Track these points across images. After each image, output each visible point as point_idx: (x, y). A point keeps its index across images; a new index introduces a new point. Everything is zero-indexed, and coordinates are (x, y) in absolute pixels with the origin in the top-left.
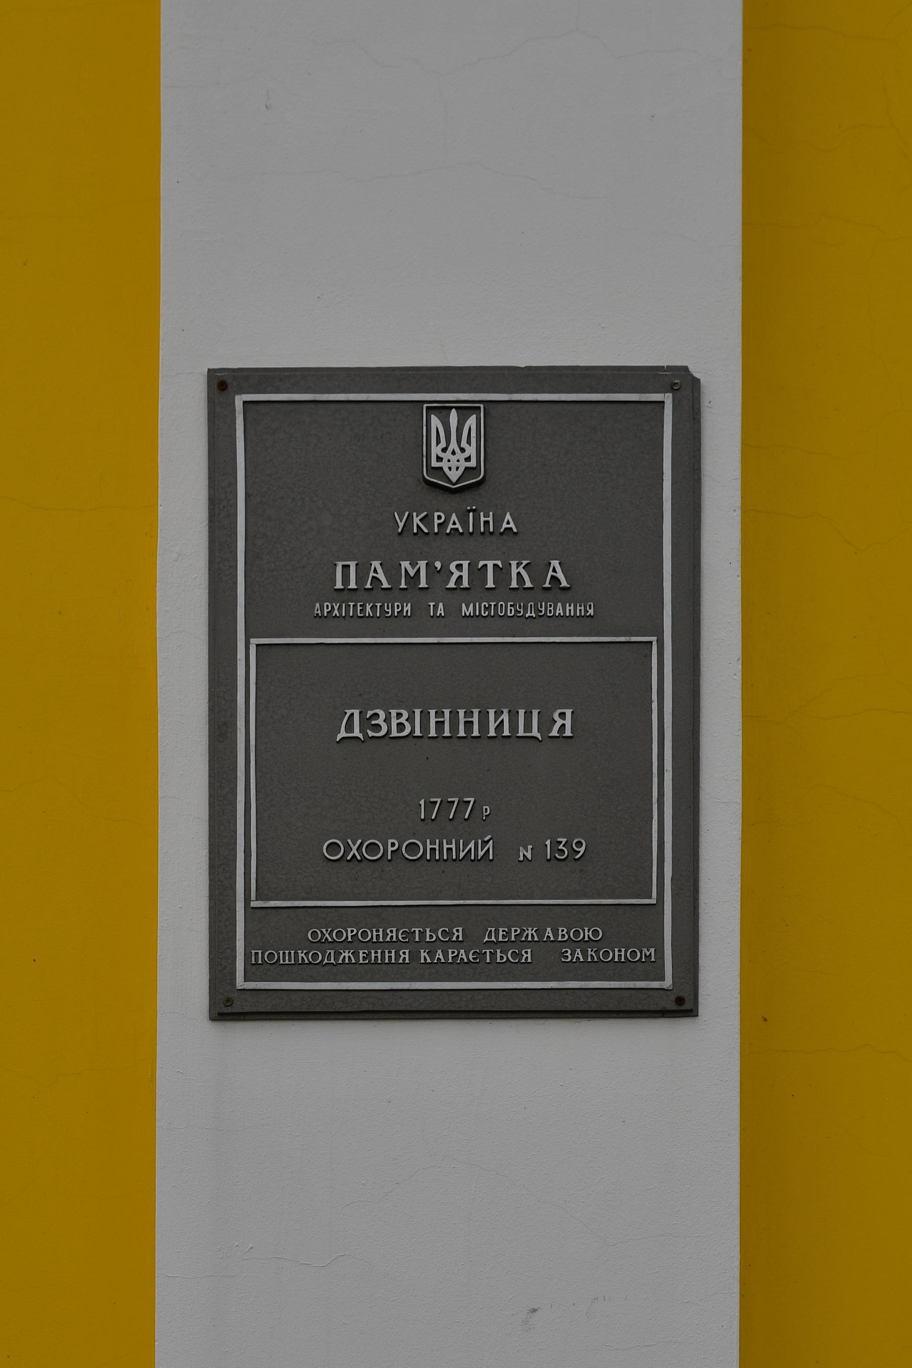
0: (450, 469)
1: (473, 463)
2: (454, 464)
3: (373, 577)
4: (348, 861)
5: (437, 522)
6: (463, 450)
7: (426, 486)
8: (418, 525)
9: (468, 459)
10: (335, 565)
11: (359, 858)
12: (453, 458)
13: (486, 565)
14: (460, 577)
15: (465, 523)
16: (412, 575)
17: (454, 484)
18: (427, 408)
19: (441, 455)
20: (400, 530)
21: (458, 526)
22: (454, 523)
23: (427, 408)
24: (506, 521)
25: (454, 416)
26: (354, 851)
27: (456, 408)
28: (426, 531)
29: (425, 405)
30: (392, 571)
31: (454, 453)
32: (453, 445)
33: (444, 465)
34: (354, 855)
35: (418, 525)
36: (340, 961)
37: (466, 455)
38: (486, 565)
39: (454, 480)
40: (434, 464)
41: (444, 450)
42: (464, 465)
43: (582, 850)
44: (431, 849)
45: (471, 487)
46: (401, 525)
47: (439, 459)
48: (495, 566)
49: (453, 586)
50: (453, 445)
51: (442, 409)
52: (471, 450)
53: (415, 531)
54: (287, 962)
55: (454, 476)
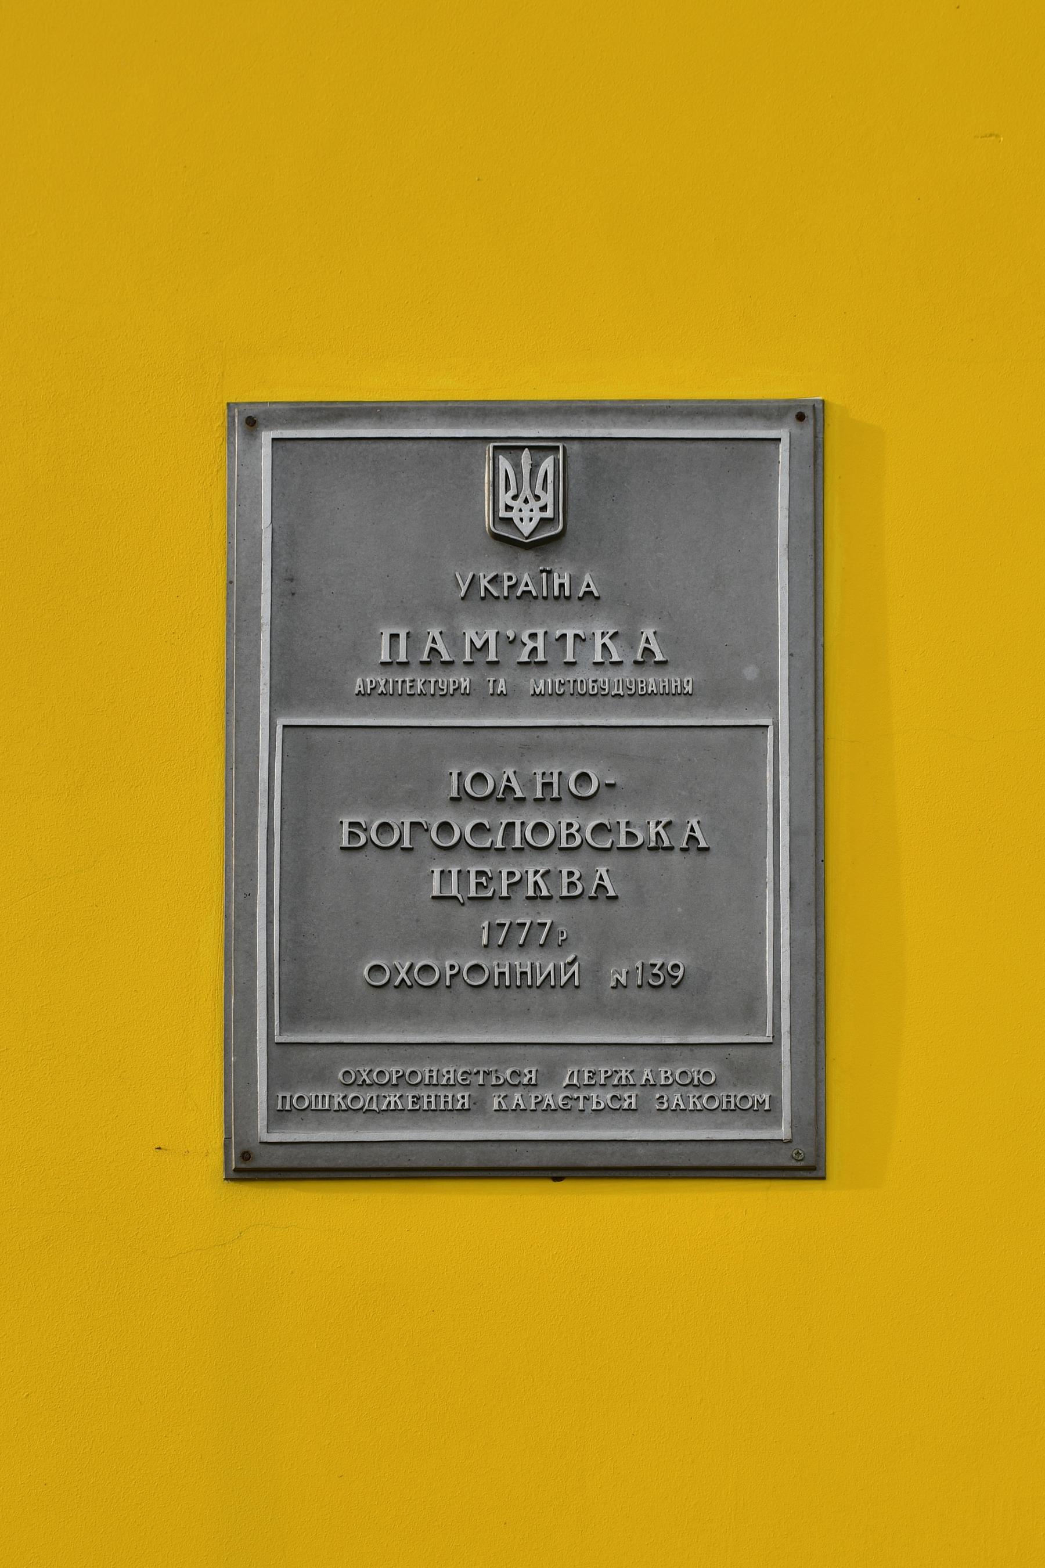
0: (522, 520)
1: (549, 513)
2: (526, 514)
3: (432, 649)
4: (396, 987)
5: (506, 583)
6: (537, 498)
7: (492, 541)
8: (486, 588)
9: (543, 509)
10: (342, 823)
11: (409, 983)
12: (526, 508)
13: (564, 636)
14: (535, 649)
15: (538, 584)
16: (478, 646)
17: (527, 538)
18: (494, 447)
19: (510, 503)
20: (462, 594)
21: (530, 588)
22: (527, 585)
23: (494, 447)
24: (585, 584)
25: (525, 457)
26: (403, 975)
27: (530, 448)
28: (496, 594)
29: (491, 445)
30: (454, 640)
31: (526, 501)
32: (526, 492)
33: (514, 515)
34: (403, 980)
35: (486, 588)
36: (384, 1108)
37: (541, 503)
38: (564, 636)
39: (526, 535)
40: (502, 513)
41: (515, 498)
42: (537, 516)
43: (680, 973)
44: (500, 973)
45: (542, 545)
46: (464, 589)
47: (508, 508)
48: (576, 636)
49: (526, 659)
50: (526, 492)
51: (510, 448)
52: (548, 498)
53: (483, 595)
54: (320, 1107)
55: (527, 528)
